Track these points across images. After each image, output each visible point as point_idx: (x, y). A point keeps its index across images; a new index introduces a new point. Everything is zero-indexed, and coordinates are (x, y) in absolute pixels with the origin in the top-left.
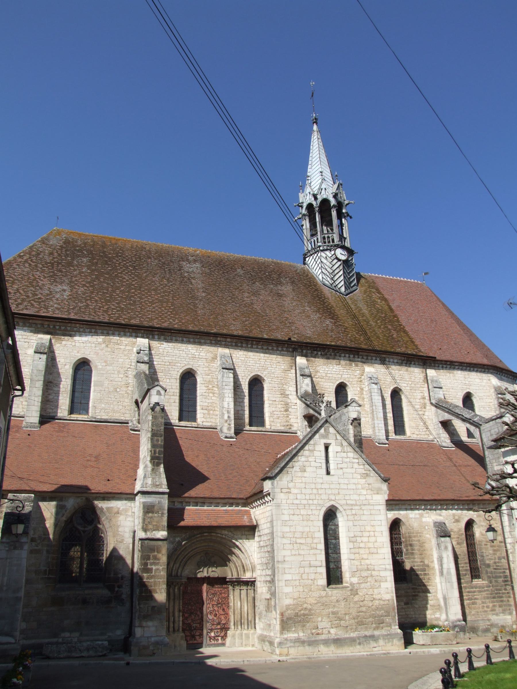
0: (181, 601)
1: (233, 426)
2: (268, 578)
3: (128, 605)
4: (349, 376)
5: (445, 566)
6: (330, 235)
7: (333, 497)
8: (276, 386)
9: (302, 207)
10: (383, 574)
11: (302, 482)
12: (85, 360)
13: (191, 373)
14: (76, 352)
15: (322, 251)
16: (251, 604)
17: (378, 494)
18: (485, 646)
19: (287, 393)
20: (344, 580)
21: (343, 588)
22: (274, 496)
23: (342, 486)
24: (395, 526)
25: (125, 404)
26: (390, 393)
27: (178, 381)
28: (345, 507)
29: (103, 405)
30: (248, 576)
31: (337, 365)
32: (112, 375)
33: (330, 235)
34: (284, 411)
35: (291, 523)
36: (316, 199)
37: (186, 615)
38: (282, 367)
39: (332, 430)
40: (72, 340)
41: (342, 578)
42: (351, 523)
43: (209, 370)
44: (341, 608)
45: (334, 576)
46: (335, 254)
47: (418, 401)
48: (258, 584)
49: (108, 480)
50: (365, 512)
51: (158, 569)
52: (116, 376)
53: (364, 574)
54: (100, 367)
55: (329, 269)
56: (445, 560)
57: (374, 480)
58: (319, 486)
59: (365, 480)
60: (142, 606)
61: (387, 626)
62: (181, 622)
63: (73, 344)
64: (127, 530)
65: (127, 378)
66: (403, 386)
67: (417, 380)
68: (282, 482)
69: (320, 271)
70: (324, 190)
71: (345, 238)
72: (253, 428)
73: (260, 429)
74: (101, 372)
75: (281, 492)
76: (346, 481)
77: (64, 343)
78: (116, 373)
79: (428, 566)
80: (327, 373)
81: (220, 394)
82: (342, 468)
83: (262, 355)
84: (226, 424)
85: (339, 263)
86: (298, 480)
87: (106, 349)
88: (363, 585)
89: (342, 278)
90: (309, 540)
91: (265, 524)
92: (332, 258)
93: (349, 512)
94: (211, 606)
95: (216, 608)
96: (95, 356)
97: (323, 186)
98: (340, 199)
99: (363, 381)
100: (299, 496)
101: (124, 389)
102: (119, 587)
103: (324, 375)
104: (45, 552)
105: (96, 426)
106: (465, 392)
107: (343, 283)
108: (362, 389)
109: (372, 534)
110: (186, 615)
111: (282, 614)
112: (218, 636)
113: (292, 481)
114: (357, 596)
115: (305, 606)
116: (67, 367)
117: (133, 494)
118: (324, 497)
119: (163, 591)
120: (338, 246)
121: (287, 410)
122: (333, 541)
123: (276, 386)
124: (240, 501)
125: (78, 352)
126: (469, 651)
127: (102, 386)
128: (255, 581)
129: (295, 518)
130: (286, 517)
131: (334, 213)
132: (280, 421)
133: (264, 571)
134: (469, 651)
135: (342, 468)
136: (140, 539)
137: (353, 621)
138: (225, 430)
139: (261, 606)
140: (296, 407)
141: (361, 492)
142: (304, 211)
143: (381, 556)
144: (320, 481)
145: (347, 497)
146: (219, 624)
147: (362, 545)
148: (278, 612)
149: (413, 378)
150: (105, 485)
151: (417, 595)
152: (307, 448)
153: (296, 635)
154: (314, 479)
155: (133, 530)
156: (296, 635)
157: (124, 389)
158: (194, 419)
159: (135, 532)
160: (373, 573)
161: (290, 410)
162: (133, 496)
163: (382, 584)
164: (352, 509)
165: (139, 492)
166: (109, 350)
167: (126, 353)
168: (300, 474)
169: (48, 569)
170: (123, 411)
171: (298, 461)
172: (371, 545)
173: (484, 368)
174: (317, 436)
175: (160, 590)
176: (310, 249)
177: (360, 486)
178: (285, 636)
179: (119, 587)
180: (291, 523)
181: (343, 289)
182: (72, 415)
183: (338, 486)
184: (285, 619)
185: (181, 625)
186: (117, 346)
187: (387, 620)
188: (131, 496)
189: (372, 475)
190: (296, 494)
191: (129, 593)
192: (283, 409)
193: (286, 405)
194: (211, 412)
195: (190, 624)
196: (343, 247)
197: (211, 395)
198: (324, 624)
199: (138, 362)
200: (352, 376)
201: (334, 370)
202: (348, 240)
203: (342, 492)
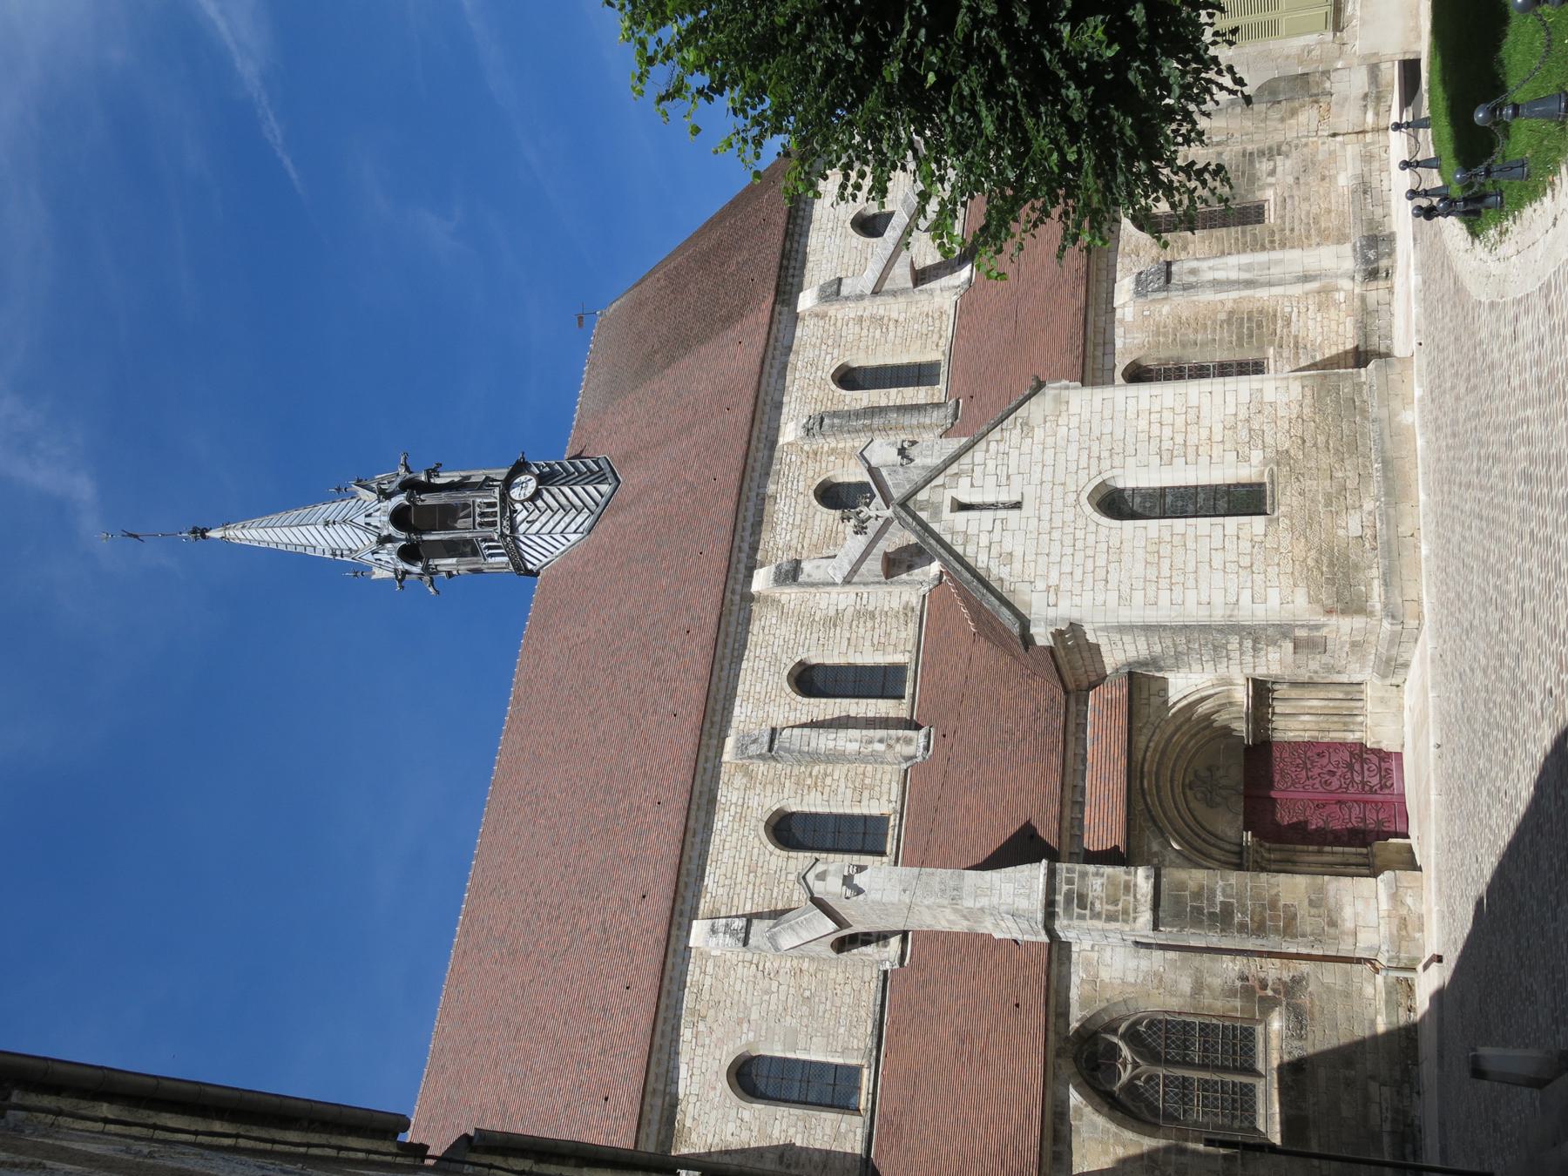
0: (1299, 847)
1: (900, 733)
2: (1248, 643)
3: (1305, 967)
5: (1233, 275)
6: (478, 510)
7: (1071, 497)
8: (815, 636)
9: (406, 572)
10: (1244, 398)
13: (778, 823)
14: (712, 1094)
16: (1306, 693)
18: (1403, 169)
19: (832, 613)
20: (1255, 479)
21: (1272, 482)
23: (1048, 477)
24: (1137, 374)
25: (840, 978)
28: (1093, 472)
29: (842, 1030)
30: (1242, 695)
33: (478, 510)
34: (878, 623)
35: (1125, 589)
39: (922, 496)
41: (1251, 485)
42: (1131, 461)
44: (1318, 486)
45: (1245, 500)
46: (522, 502)
47: (865, 332)
48: (1261, 672)
50: (1107, 430)
51: (1224, 891)
52: (774, 997)
54: (751, 1035)
55: (557, 517)
56: (1221, 275)
57: (1036, 409)
58: (1045, 525)
60: (1308, 930)
61: (1361, 392)
63: (693, 1099)
64: (1132, 964)
71: (487, 478)
72: (908, 691)
73: (910, 674)
75: (1055, 605)
76: (1038, 468)
78: (766, 997)
79: (1231, 313)
81: (828, 761)
82: (1008, 477)
83: (744, 665)
84: (898, 747)
85: (546, 495)
86: (1030, 570)
88: (1269, 440)
89: (578, 489)
90: (1165, 550)
91: (1127, 647)
93: (1105, 464)
95: (1316, 771)
97: (361, 520)
98: (394, 486)
102: (1264, 986)
103: (796, 532)
105: (888, 1048)
106: (851, 231)
107: (590, 488)
108: (833, 451)
109: (1155, 417)
111: (1329, 612)
112: (1380, 768)
114: (1292, 452)
115: (1310, 562)
116: (746, 1115)
117: (1050, 945)
118: (1069, 516)
119: (1273, 881)
120: (505, 496)
122: (1169, 500)
123: (815, 636)
124: (1073, 708)
126: (1406, 165)
127: (796, 1032)
128: (1254, 680)
129: (1113, 578)
130: (1112, 597)
131: (429, 499)
133: (1232, 655)
134: (1406, 165)
135: (1008, 477)
136: (1156, 927)
137: (1347, 462)
138: (909, 750)
139: (1312, 666)
142: (417, 569)
143: (1206, 400)
145: (1073, 467)
147: (1179, 439)
148: (1323, 619)
150: (1029, 1011)
151: (1296, 337)
152: (959, 549)
153: (1376, 583)
155: (1132, 949)
156: (1376, 583)
158: (882, 821)
159: (1137, 943)
160: (1241, 417)
161: (870, 608)
162: (1055, 948)
163: (1266, 399)
164: (1099, 458)
167: (721, 974)
168: (1017, 566)
170: (857, 984)
171: (988, 569)
172: (1180, 421)
174: (935, 527)
175: (1271, 886)
177: (1050, 441)
178: (1378, 607)
179: (1264, 986)
180: (1125, 589)
181: (604, 488)
184: (1339, 606)
185: (1353, 850)
186: (705, 995)
187: (1346, 389)
188: (1058, 951)
191: (1277, 961)
192: (870, 624)
194: (867, 781)
196: (508, 484)
197: (828, 781)
198: (1353, 524)
199: (745, 943)
202: (493, 473)
203: (1060, 477)
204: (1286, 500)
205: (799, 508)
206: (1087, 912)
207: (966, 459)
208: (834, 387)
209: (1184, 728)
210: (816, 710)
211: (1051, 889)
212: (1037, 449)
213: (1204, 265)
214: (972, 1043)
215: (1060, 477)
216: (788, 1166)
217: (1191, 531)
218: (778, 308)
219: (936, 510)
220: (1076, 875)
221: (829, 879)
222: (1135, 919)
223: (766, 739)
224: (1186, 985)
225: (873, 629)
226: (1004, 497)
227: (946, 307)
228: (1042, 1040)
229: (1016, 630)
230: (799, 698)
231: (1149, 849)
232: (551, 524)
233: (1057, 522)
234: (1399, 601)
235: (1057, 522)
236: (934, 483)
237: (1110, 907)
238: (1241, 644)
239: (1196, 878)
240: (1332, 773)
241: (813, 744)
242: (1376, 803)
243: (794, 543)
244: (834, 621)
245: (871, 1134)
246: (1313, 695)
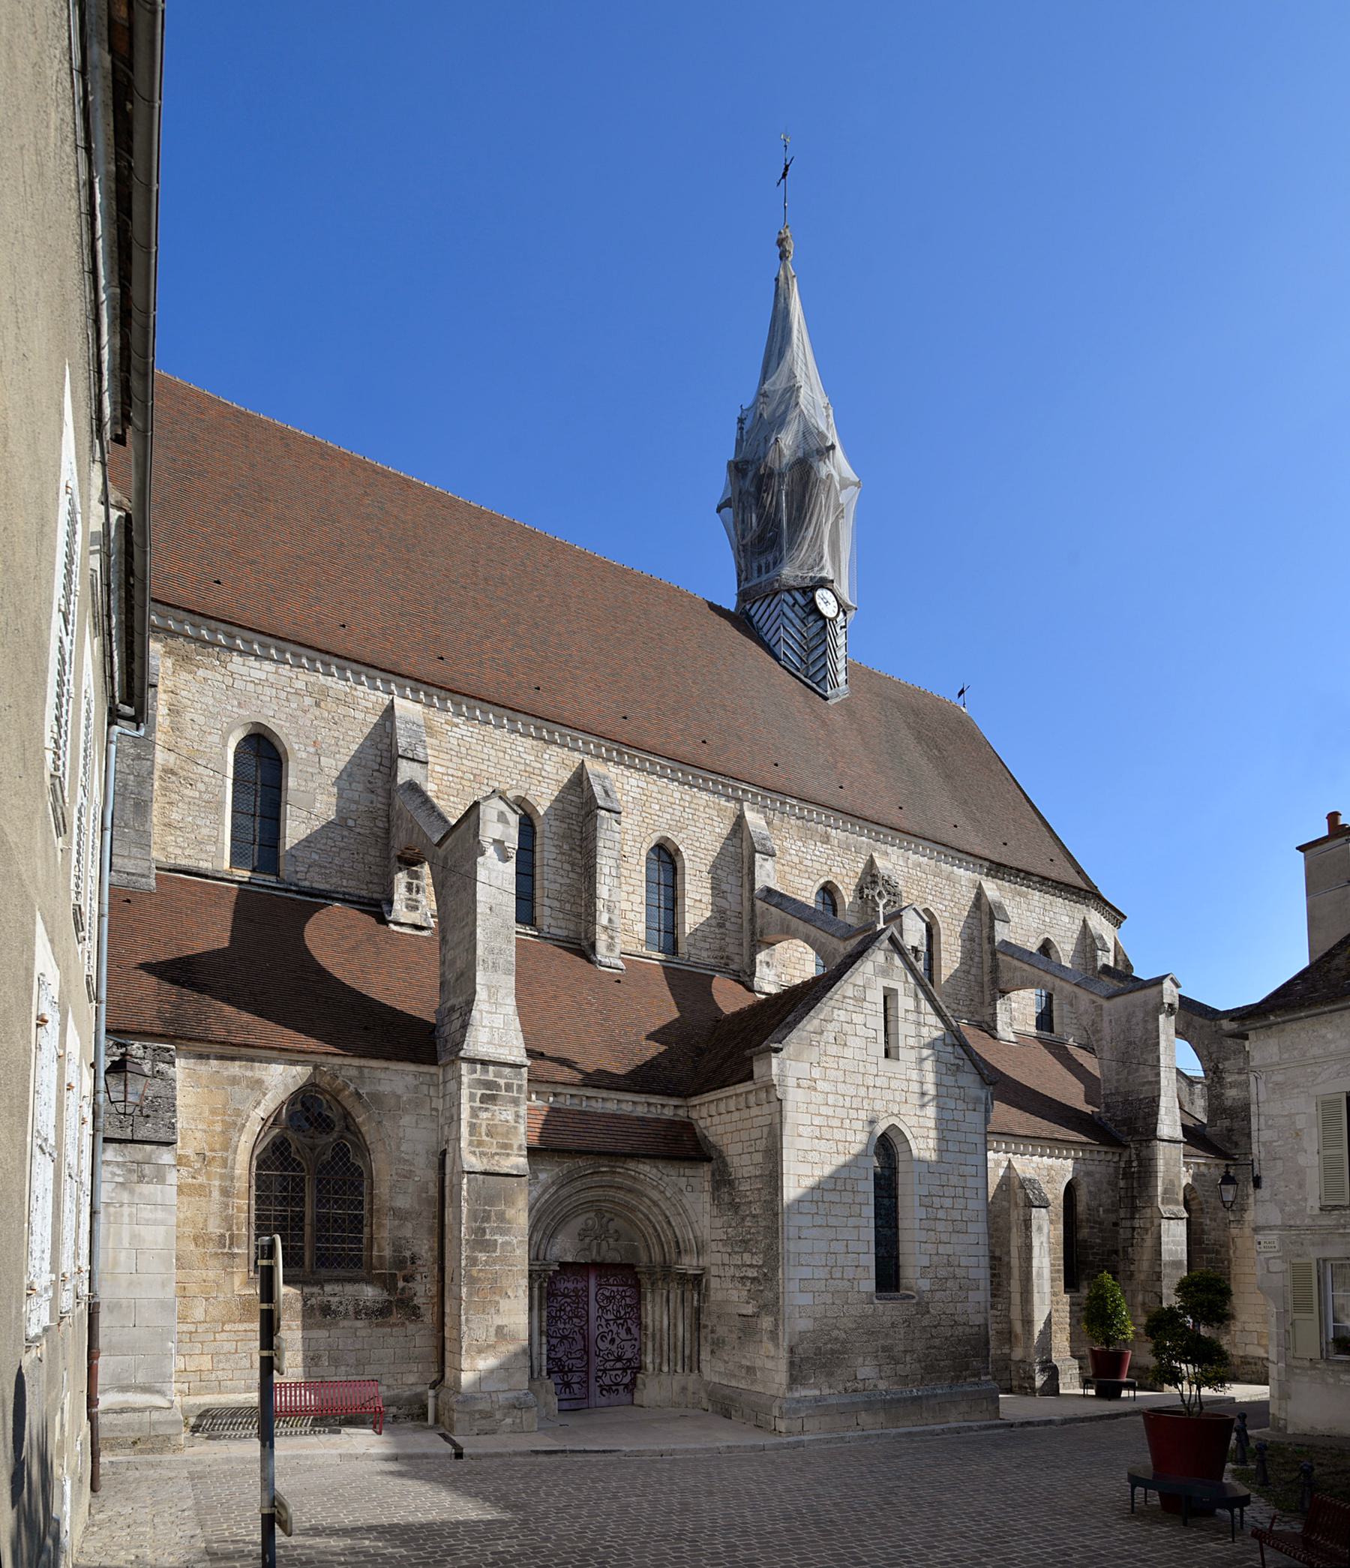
3: (429, 1317)
12: (261, 731)
20: (903, 1282)
29: (315, 856)
30: (688, 1263)
37: (554, 1341)
38: (718, 830)
45: (888, 1275)
53: (942, 1273)
54: (304, 755)
61: (974, 1376)
62: (545, 1357)
75: (798, 1086)
88: (938, 1295)
90: (847, 1197)
94: (603, 1323)
95: (614, 1328)
100: (831, 1099)
103: (796, 860)
104: (216, 1194)
106: (1042, 937)
110: (554, 1341)
111: (792, 1350)
112: (617, 1384)
125: (240, 705)
129: (822, 1145)
143: (973, 1239)
146: (619, 1359)
147: (941, 1214)
148: (785, 1344)
156: (817, 1393)
159: (444, 1153)
168: (833, 1050)
169: (227, 1234)
178: (797, 1395)
195: (560, 1359)
197: (567, 867)
204: (889, 1310)
205: (817, 865)
206: (478, 1104)
209: (655, 1209)
213: (1044, 1239)
217: (863, 1222)
218: (987, 864)
220: (515, 1094)
221: (500, 826)
222: (474, 1153)
224: (403, 1202)
231: (541, 1171)
234: (803, 1415)
237: (483, 1130)
238: (751, 1266)
239: (519, 1217)
240: (613, 1341)
242: (587, 1382)
245: (207, 877)
246: (687, 1327)
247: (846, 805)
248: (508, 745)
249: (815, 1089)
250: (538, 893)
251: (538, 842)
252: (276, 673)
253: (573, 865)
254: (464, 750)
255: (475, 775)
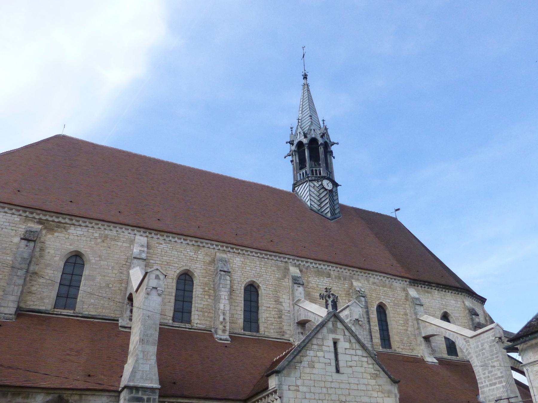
4: (338, 289)
8: (271, 293)
11: (311, 380)
14: (68, 244)
15: (310, 181)
17: (389, 397)
19: (281, 300)
22: (282, 393)
26: (375, 307)
27: (175, 281)
29: (92, 301)
31: (327, 277)
32: (106, 271)
36: (305, 137)
38: (277, 276)
39: (339, 325)
40: (65, 233)
43: (206, 273)
46: (322, 184)
47: (401, 316)
49: (89, 376)
54: (94, 261)
55: (316, 197)
58: (328, 385)
59: (375, 381)
63: (67, 236)
65: (122, 275)
66: (386, 302)
67: (399, 297)
68: (290, 378)
69: (309, 198)
70: (313, 130)
74: (94, 266)
75: (289, 390)
76: (356, 381)
77: (56, 234)
78: (110, 268)
80: (318, 285)
81: (215, 296)
82: (351, 367)
84: (221, 327)
85: (325, 192)
87: (103, 244)
89: (328, 205)
92: (320, 188)
96: (89, 250)
97: (312, 128)
99: (351, 294)
101: (118, 285)
103: (315, 286)
106: (442, 311)
107: (328, 209)
113: (300, 377)
120: (325, 178)
121: (280, 317)
123: (271, 293)
125: (71, 245)
131: (321, 150)
132: (273, 327)
135: (351, 367)
138: (220, 332)
140: (289, 315)
141: (371, 394)
144: (330, 379)
149: (396, 295)
154: (323, 376)
157: (118, 285)
162: (116, 394)
165: (126, 387)
166: (105, 245)
167: (122, 249)
168: (308, 370)
173: (457, 291)
174: (325, 330)
176: (299, 179)
181: (329, 215)
182: (56, 310)
183: (347, 386)
186: (113, 243)
189: (381, 375)
190: (305, 392)
192: (276, 316)
193: (279, 311)
194: (206, 314)
197: (207, 297)
200: (341, 289)
201: (324, 282)
203: (353, 393)
207: (357, 346)
208: (377, 303)
210: (238, 292)
211: (145, 389)
212: (365, 381)
214: (76, 355)
215: (353, 393)
216: (31, 276)
218: (408, 280)
219: (334, 331)
221: (156, 281)
223: (226, 269)
225: (274, 318)
226: (341, 364)
227: (415, 352)
228: (68, 387)
229: (277, 368)
230: (243, 285)
232: (314, 195)
233: (331, 391)
235: (331, 391)
236: (346, 331)
241: (223, 289)
243: (311, 285)
244: (278, 302)
245: (42, 313)
247: (337, 260)
248: (183, 250)
249: (299, 391)
250: (193, 309)
251: (194, 287)
252: (88, 231)
253: (209, 296)
254: (163, 253)
255: (167, 263)
